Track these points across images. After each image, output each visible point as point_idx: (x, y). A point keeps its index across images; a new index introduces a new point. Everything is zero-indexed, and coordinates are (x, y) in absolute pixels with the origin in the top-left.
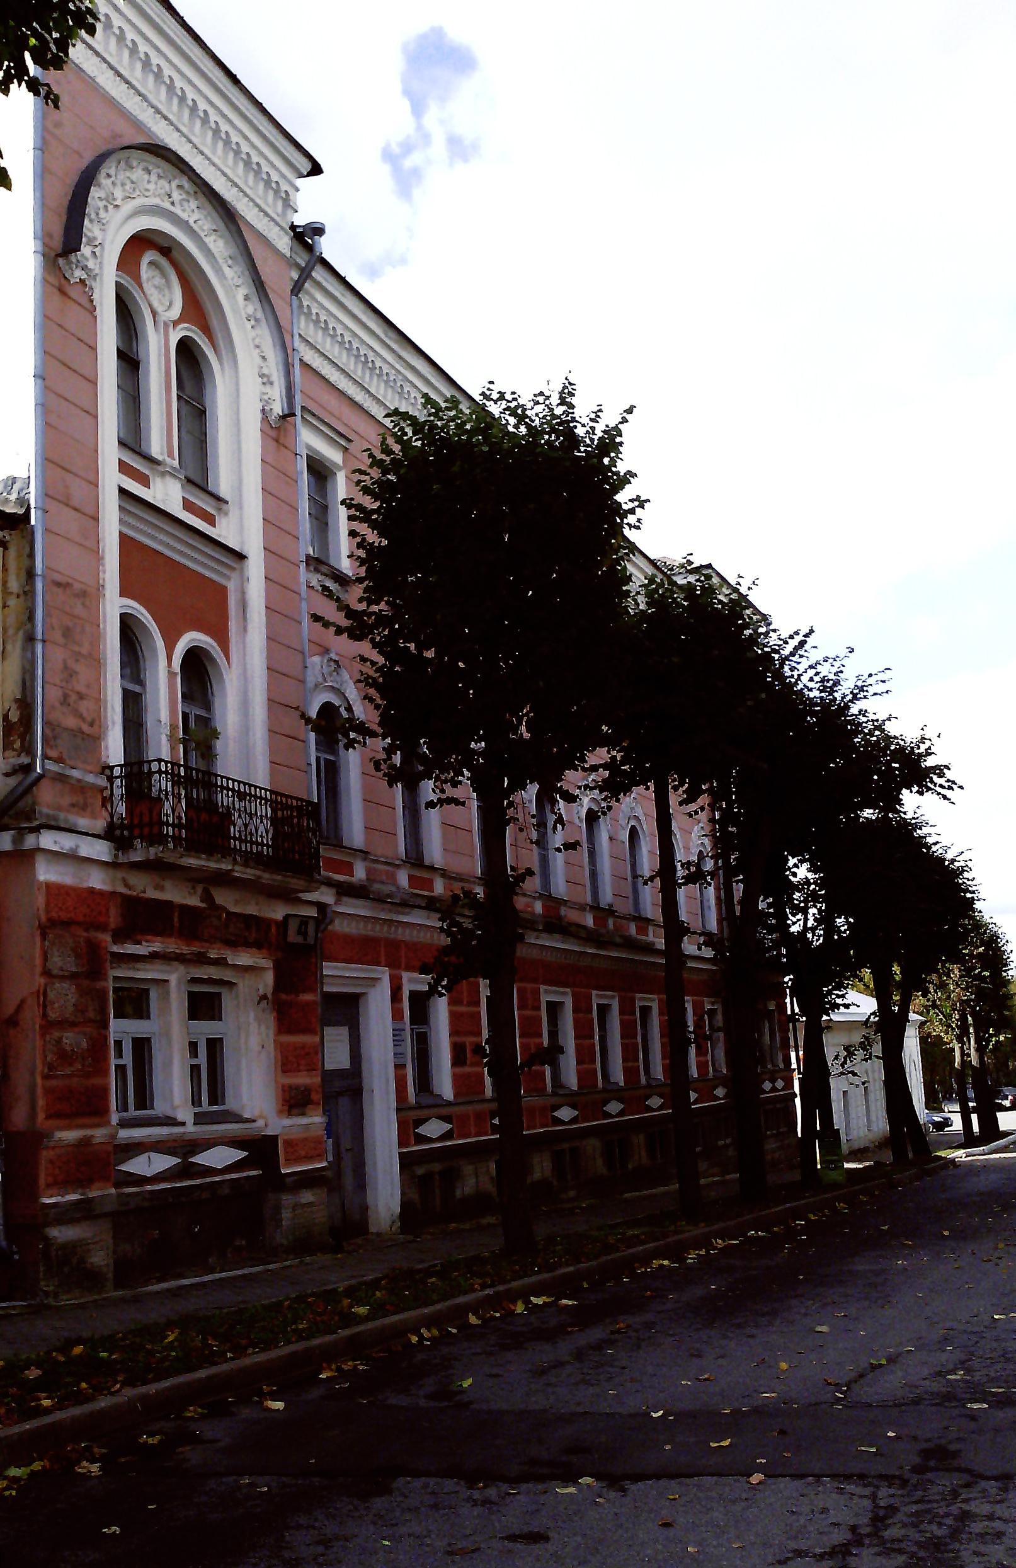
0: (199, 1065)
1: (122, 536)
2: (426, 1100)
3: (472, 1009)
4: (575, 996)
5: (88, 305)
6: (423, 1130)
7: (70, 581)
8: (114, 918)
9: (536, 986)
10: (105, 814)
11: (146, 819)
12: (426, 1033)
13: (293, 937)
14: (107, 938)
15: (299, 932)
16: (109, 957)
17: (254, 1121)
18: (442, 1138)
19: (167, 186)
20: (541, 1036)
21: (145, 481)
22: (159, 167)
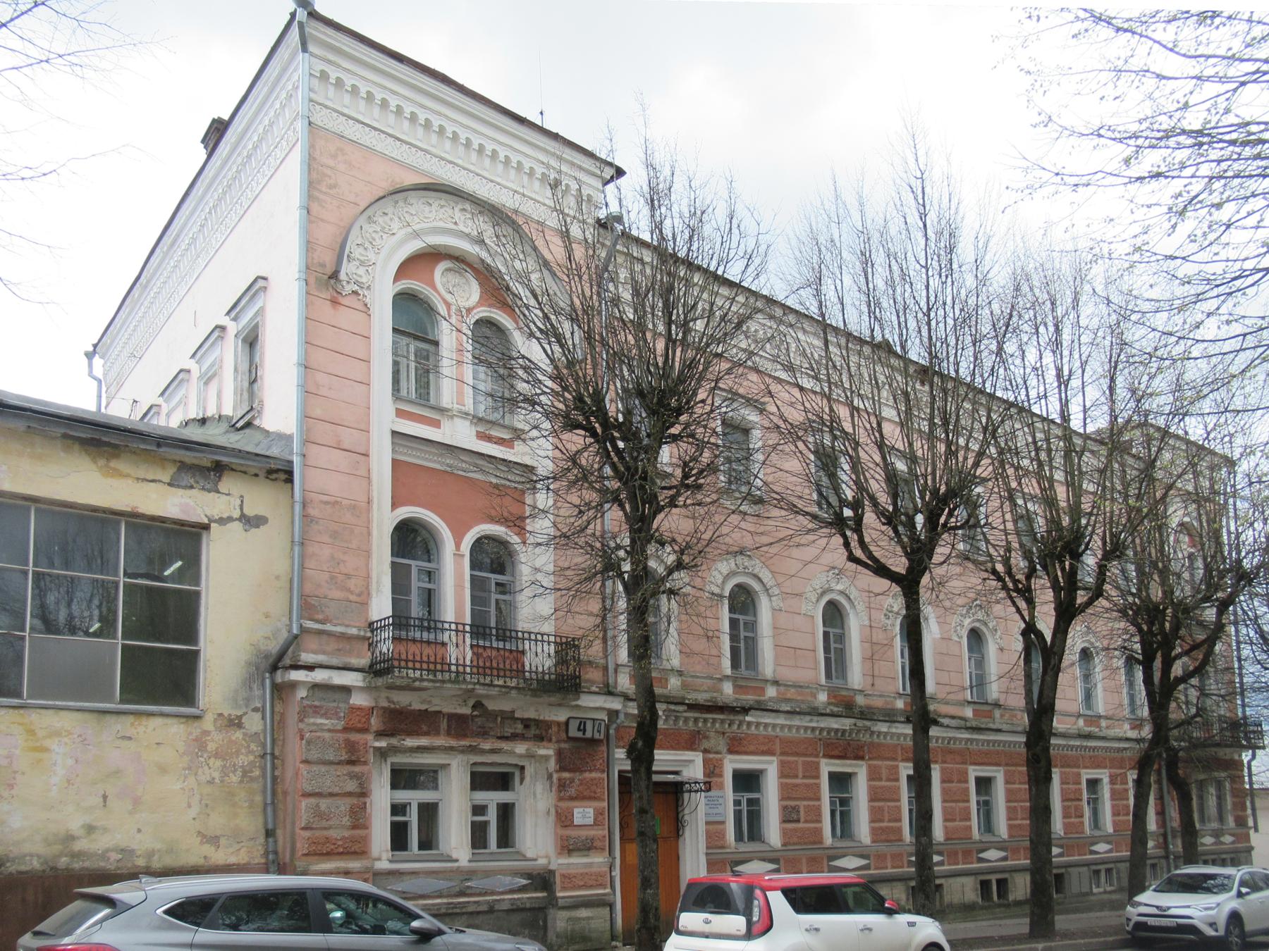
0: (486, 824)
1: (395, 463)
2: (1097, 833)
3: (1077, 787)
4: (1006, 773)
5: (364, 309)
6: (1095, 848)
7: (339, 499)
8: (375, 722)
9: (1075, 770)
10: (369, 654)
11: (432, 659)
12: (758, 799)
13: (574, 732)
14: (370, 737)
15: (579, 729)
16: (372, 750)
17: (536, 860)
18: (1106, 852)
19: (450, 211)
20: (1128, 799)
21: (436, 424)
22: (437, 201)
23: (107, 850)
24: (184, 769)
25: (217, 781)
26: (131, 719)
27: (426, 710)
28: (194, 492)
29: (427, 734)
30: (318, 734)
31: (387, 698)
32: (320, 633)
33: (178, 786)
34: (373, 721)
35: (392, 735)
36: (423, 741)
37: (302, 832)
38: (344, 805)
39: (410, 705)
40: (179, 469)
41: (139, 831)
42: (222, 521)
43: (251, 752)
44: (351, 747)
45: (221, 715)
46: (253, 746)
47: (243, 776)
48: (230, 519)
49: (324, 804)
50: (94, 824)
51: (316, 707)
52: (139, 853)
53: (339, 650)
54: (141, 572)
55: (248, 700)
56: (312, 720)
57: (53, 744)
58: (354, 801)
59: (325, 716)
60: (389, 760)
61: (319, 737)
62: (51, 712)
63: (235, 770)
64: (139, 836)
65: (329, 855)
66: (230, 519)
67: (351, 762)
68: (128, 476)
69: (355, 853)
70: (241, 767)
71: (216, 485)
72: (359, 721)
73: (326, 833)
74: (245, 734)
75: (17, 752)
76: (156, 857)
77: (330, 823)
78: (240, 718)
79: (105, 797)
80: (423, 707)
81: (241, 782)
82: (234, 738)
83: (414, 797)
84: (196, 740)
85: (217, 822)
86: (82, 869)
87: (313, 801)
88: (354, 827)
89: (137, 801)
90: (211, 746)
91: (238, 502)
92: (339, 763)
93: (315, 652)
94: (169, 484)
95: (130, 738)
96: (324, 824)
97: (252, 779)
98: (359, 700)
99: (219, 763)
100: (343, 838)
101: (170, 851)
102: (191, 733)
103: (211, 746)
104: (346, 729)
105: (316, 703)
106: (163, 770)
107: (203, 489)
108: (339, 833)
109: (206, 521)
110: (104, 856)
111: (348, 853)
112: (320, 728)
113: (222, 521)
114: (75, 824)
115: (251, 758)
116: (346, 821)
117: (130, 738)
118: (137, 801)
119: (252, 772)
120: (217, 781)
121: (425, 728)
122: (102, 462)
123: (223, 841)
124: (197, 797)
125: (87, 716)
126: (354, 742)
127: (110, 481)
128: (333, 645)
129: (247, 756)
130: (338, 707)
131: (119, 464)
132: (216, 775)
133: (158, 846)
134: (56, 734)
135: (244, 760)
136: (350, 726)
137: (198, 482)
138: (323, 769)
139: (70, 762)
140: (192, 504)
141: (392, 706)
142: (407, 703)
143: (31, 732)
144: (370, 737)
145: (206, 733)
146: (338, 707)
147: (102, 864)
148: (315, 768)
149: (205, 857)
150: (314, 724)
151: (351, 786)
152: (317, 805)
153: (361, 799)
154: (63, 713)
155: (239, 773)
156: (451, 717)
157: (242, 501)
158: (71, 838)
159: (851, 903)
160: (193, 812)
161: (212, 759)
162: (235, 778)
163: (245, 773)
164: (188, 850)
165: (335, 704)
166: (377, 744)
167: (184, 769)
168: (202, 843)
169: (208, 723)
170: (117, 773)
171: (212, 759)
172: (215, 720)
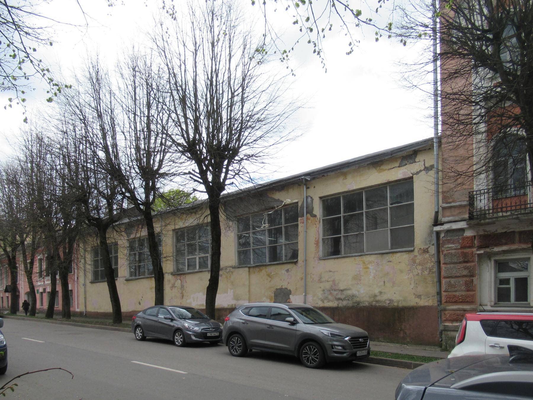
16: (476, 255)
23: (386, 300)
24: (408, 271)
25: (420, 274)
26: (391, 255)
27: (506, 232)
28: (407, 166)
29: (506, 244)
30: (450, 251)
31: (483, 230)
32: (450, 207)
33: (407, 277)
34: (476, 242)
35: (487, 247)
36: (505, 248)
37: (444, 293)
38: (462, 281)
39: (496, 231)
40: (402, 160)
41: (395, 293)
42: (417, 173)
43: (432, 262)
44: (465, 255)
45: (420, 249)
46: (433, 260)
47: (429, 272)
48: (421, 171)
49: (453, 281)
50: (382, 291)
51: (449, 240)
52: (395, 301)
53: (460, 213)
54: (394, 202)
55: (430, 241)
56: (447, 246)
57: (370, 266)
58: (467, 279)
59: (453, 243)
60: (493, 260)
61: (450, 253)
62: (368, 256)
63: (427, 269)
64: (395, 295)
65: (456, 302)
66: (421, 171)
67: (465, 262)
68: (386, 170)
69: (467, 302)
70: (429, 268)
71: (415, 160)
72: (468, 243)
73: (454, 293)
74: (430, 255)
75: (361, 269)
76: (400, 303)
77: (456, 289)
78: (427, 249)
79: (384, 282)
80: (504, 231)
81: (429, 274)
82: (425, 257)
83: (511, 276)
84: (412, 259)
85: (420, 290)
86: (379, 306)
87: (448, 280)
88: (468, 291)
89: (394, 283)
90: (417, 261)
91: (423, 163)
92: (460, 263)
93: (448, 216)
94: (399, 167)
95: (391, 261)
96: (453, 289)
97: (433, 273)
98: (469, 233)
99: (420, 267)
100: (462, 296)
101: (405, 300)
102: (410, 257)
103: (417, 261)
104: (462, 248)
105: (449, 238)
106: (401, 271)
107: (410, 163)
108: (460, 293)
109: (411, 175)
110: (385, 302)
111: (464, 302)
112: (451, 248)
113: (417, 173)
114: (377, 291)
115: (432, 264)
116: (463, 288)
117: (391, 261)
118: (394, 283)
119: (433, 269)
120: (420, 274)
121: (504, 241)
122: (378, 168)
123: (422, 297)
124: (413, 281)
125: (378, 256)
126: (466, 253)
127: (382, 174)
128: (457, 211)
129: (431, 263)
130: (459, 238)
131: (383, 167)
132: (420, 272)
133: (401, 299)
134: (370, 262)
135: (429, 265)
136: (463, 246)
137: (408, 162)
138: (452, 266)
139: (374, 271)
140: (406, 171)
141: (486, 233)
142: (495, 230)
143: (364, 263)
144: (474, 250)
145: (416, 256)
146: (459, 238)
147: (384, 304)
148: (449, 266)
149: (417, 303)
150: (448, 247)
151: (465, 272)
152: (450, 281)
153: (471, 278)
154: (371, 256)
155: (428, 270)
156: (521, 233)
157: (424, 162)
158: (376, 296)
159: (216, 318)
160: (412, 286)
161: (418, 266)
162: (426, 273)
163: (430, 270)
164: (410, 300)
165: (457, 237)
166: (478, 252)
167: (408, 271)
168: (415, 298)
169: (416, 253)
170: (388, 274)
171: (418, 266)
172: (418, 251)
